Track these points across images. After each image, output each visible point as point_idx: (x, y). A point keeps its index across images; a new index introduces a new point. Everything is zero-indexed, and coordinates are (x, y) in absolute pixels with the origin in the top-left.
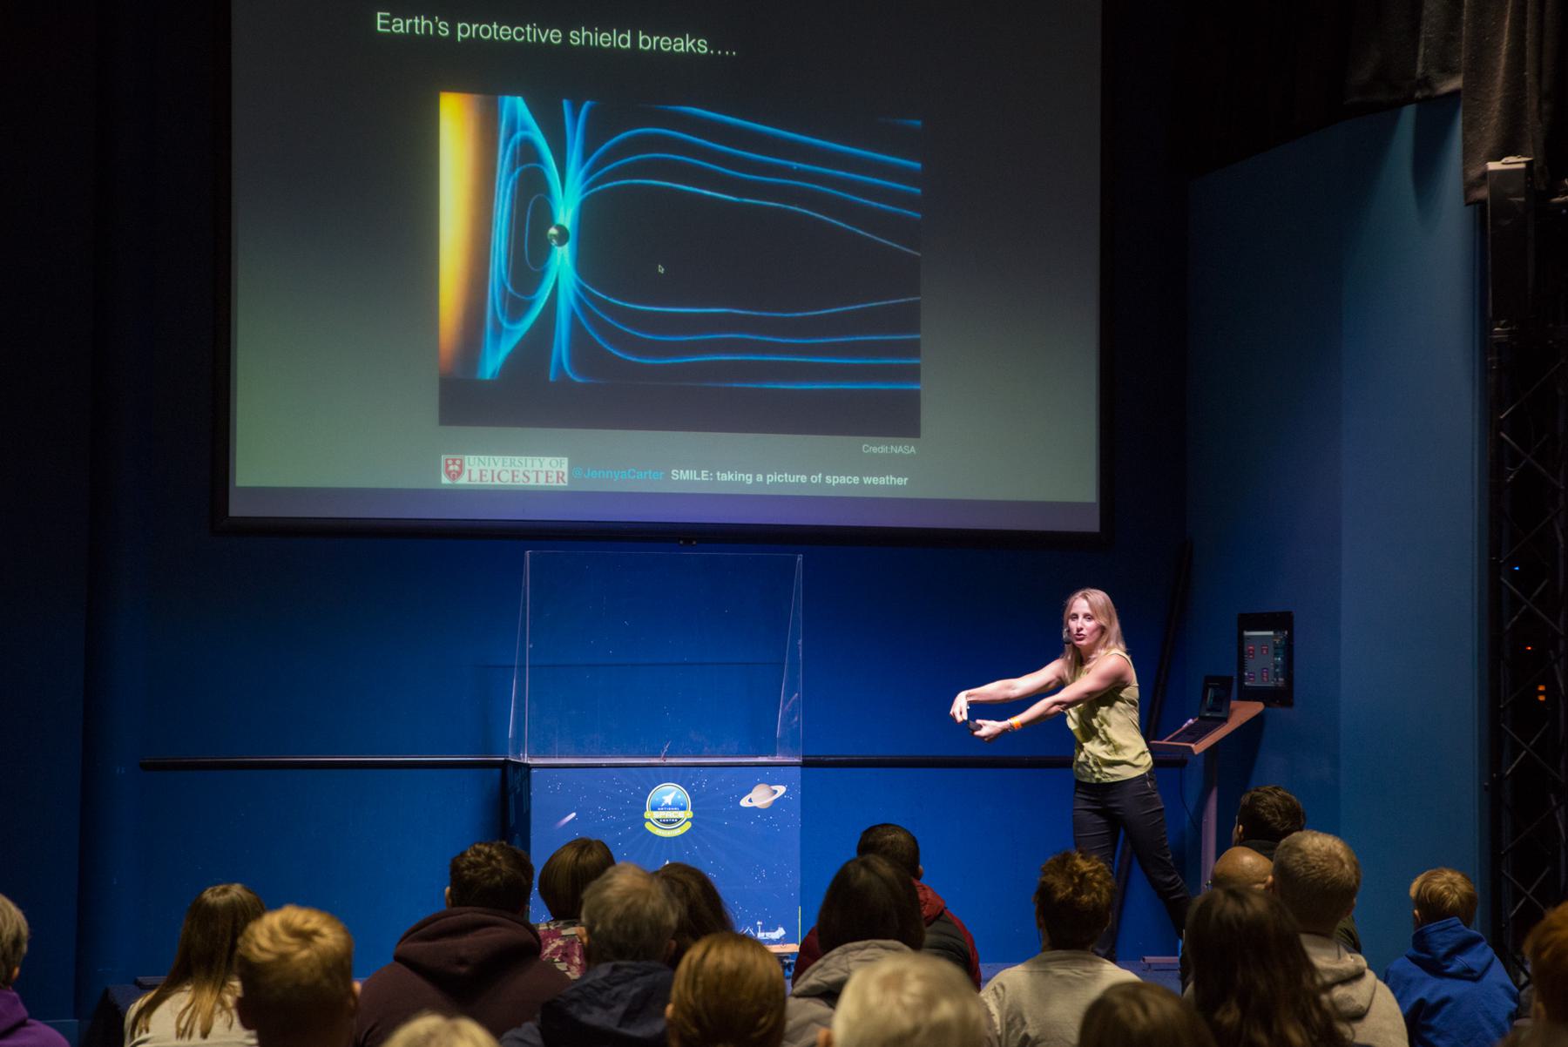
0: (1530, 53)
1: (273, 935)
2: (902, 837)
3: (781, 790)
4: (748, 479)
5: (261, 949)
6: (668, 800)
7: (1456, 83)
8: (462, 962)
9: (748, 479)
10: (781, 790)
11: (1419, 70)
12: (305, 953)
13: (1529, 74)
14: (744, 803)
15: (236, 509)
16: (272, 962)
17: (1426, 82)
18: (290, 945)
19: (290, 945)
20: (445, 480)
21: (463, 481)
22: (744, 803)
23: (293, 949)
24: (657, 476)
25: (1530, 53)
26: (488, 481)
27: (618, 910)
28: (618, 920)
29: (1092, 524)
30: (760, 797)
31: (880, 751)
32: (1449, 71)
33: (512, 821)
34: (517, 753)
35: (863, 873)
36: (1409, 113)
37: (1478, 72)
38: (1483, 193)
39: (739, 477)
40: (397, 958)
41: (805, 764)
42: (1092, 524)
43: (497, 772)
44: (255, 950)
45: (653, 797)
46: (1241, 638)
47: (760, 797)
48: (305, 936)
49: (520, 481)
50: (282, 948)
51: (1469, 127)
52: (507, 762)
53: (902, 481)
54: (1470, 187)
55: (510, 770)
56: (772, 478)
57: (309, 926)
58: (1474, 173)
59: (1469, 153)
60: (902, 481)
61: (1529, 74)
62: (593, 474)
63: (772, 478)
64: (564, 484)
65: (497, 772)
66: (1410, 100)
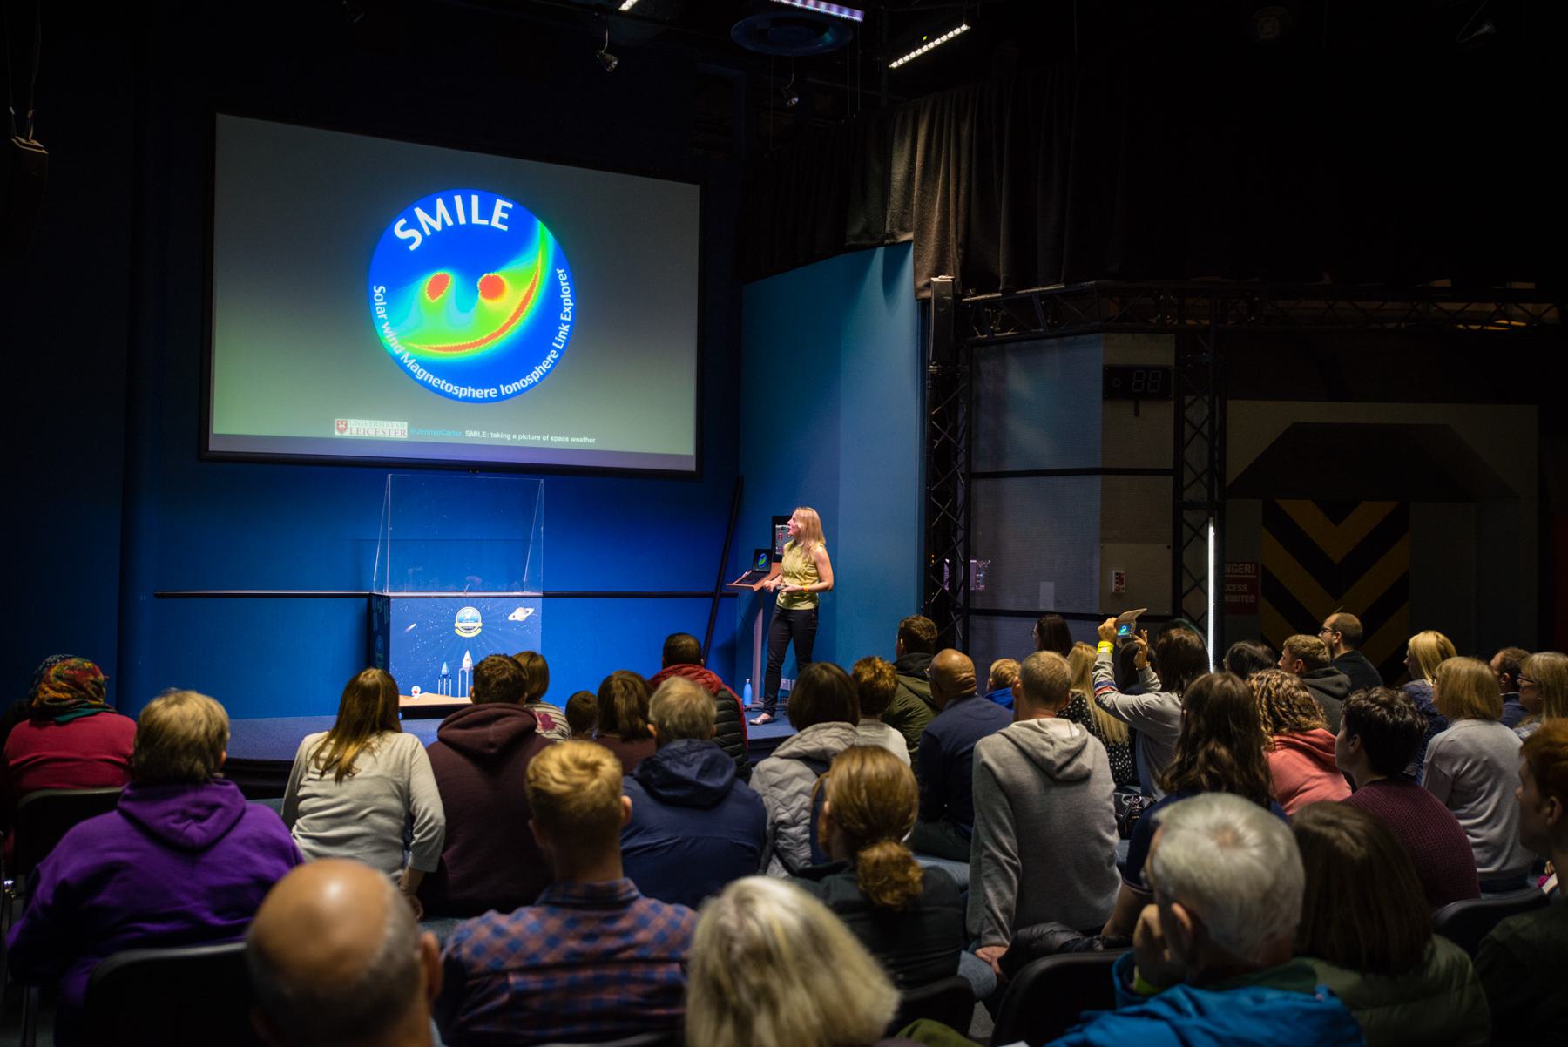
0: (952, 221)
1: (564, 769)
2: (692, 642)
3: (531, 611)
4: (508, 437)
5: (558, 782)
6: (468, 616)
7: (910, 236)
8: (492, 745)
9: (508, 437)
10: (531, 611)
11: (888, 228)
12: (595, 782)
13: (952, 234)
14: (511, 618)
15: (214, 446)
16: (566, 794)
17: (892, 235)
18: (579, 776)
19: (579, 776)
20: (337, 433)
21: (347, 434)
22: (511, 618)
23: (585, 780)
24: (458, 434)
25: (952, 221)
26: (361, 434)
27: (680, 709)
28: (680, 716)
29: (692, 467)
30: (520, 615)
31: (579, 589)
32: (904, 230)
33: (376, 627)
34: (380, 589)
35: (825, 674)
36: (880, 252)
37: (921, 231)
38: (928, 294)
39: (503, 436)
40: (441, 739)
41: (545, 596)
42: (692, 467)
43: (365, 600)
44: (553, 784)
45: (460, 615)
46: (774, 529)
47: (520, 615)
48: (593, 768)
49: (380, 435)
50: (576, 780)
51: (917, 259)
52: (370, 596)
53: (592, 441)
54: (917, 291)
55: (374, 600)
56: (521, 437)
57: (591, 759)
58: (921, 283)
59: (916, 273)
60: (592, 441)
61: (952, 234)
62: (421, 432)
63: (521, 437)
64: (405, 437)
65: (365, 600)
66: (881, 244)
